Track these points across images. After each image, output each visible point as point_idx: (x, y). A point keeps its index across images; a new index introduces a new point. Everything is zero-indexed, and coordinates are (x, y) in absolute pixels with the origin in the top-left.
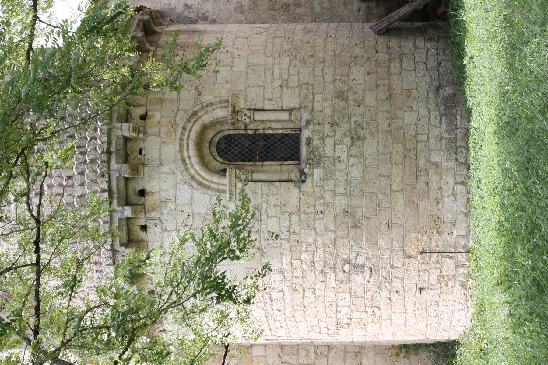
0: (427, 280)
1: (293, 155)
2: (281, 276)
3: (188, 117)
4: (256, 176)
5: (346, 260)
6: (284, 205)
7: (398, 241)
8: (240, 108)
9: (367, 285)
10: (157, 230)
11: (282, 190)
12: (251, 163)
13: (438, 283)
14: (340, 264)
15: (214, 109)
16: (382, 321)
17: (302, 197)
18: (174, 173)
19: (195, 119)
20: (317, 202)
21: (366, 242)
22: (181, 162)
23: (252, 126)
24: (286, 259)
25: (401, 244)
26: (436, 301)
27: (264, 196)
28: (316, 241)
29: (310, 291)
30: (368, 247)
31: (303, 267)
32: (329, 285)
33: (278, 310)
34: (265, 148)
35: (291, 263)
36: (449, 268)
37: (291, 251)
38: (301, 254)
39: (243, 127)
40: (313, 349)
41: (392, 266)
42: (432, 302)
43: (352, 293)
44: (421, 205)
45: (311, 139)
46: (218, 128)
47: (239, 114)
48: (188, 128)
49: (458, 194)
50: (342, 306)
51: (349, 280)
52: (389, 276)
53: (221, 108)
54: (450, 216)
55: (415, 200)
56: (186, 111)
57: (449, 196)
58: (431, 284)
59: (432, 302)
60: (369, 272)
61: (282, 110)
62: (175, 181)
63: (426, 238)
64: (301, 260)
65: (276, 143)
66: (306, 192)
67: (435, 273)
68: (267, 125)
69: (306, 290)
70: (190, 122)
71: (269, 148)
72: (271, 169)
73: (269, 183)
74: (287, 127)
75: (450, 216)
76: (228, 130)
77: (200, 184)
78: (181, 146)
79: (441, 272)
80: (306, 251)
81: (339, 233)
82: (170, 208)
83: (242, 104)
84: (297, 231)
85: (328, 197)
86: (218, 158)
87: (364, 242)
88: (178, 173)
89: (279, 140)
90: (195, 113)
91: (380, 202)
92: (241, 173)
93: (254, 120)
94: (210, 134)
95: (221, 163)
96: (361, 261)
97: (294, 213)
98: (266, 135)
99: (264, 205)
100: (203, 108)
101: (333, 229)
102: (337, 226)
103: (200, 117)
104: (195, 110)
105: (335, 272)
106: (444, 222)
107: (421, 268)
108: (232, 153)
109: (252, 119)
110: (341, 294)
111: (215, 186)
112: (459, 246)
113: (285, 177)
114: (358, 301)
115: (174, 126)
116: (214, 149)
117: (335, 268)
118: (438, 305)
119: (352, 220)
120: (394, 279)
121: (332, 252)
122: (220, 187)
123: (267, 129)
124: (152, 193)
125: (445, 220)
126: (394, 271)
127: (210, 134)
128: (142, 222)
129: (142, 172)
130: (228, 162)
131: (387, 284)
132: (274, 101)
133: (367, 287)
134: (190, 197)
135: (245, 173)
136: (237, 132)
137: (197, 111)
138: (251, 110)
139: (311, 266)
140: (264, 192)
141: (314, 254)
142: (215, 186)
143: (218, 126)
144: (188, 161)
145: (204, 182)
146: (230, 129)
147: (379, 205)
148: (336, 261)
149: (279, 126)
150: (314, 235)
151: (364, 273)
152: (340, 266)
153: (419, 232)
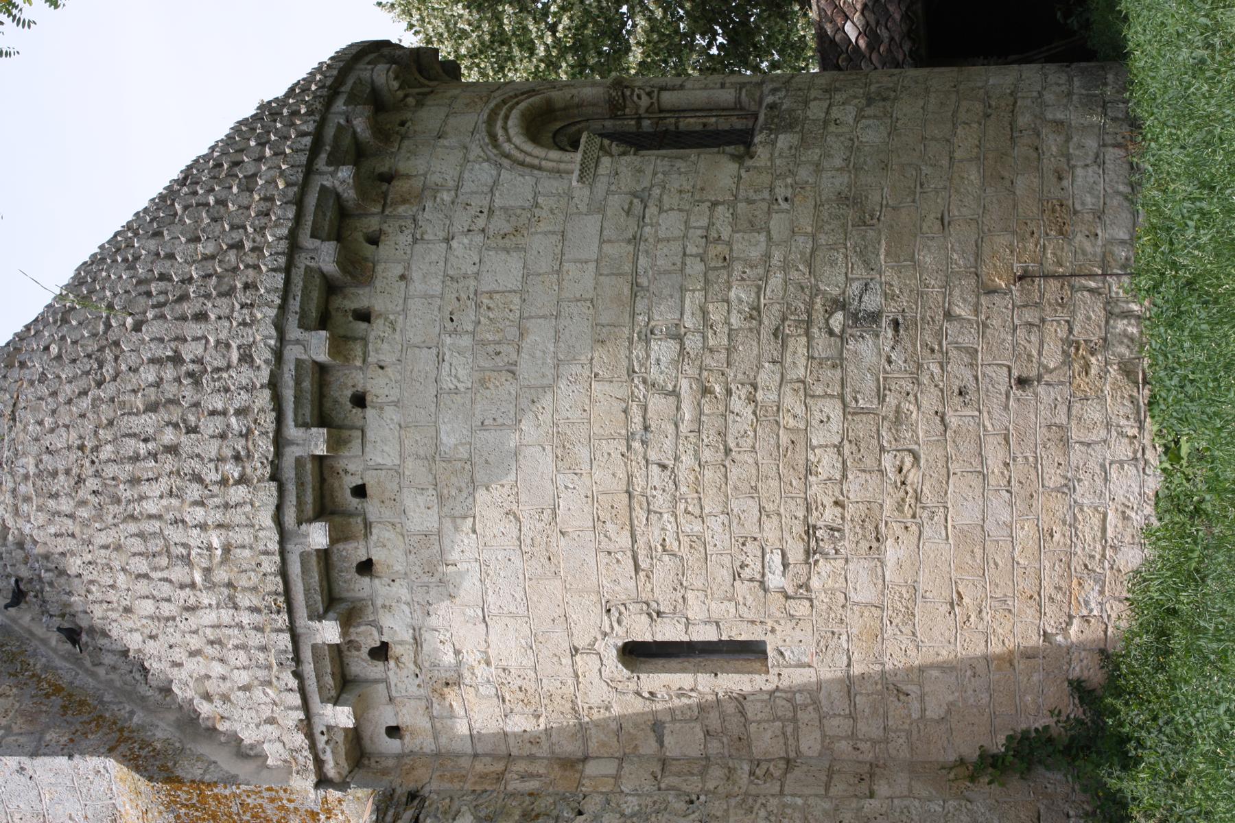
0: (1035, 353)
2: (674, 345)
5: (835, 301)
6: (702, 189)
7: (963, 252)
9: (885, 371)
10: (404, 239)
13: (1064, 363)
14: (821, 310)
16: (925, 515)
17: (743, 174)
20: (778, 183)
21: (886, 255)
24: (692, 301)
25: (972, 259)
26: (1060, 427)
28: (768, 256)
29: (743, 392)
30: (892, 268)
31: (733, 320)
32: (791, 375)
33: (659, 465)
35: (705, 312)
36: (1089, 318)
37: (707, 281)
38: (730, 288)
40: (746, 767)
41: (948, 315)
42: (1049, 427)
43: (848, 399)
44: (1020, 182)
49: (1108, 161)
50: (821, 446)
51: (842, 359)
52: (940, 345)
54: (1089, 200)
55: (1006, 174)
57: (1087, 165)
58: (1046, 367)
59: (1049, 427)
60: (890, 333)
63: (1031, 246)
64: (727, 302)
67: (1055, 332)
69: (734, 389)
75: (1089, 200)
79: (1071, 330)
80: (743, 279)
81: (823, 239)
82: (442, 200)
84: (725, 236)
85: (804, 174)
87: (882, 257)
91: (924, 179)
96: (872, 302)
97: (723, 203)
99: (656, 191)
101: (809, 229)
102: (820, 223)
105: (807, 333)
106: (1076, 212)
107: (1020, 318)
110: (820, 403)
112: (1113, 264)
114: (862, 427)
117: (809, 323)
118: (1065, 442)
119: (856, 211)
120: (953, 353)
121: (804, 281)
124: (408, 176)
125: (1078, 207)
126: (951, 328)
128: (373, 223)
129: (396, 145)
131: (936, 369)
133: (885, 379)
139: (751, 317)
141: (759, 288)
145: (528, 159)
147: (922, 185)
148: (811, 304)
150: (764, 245)
151: (878, 336)
152: (821, 317)
153: (1014, 232)
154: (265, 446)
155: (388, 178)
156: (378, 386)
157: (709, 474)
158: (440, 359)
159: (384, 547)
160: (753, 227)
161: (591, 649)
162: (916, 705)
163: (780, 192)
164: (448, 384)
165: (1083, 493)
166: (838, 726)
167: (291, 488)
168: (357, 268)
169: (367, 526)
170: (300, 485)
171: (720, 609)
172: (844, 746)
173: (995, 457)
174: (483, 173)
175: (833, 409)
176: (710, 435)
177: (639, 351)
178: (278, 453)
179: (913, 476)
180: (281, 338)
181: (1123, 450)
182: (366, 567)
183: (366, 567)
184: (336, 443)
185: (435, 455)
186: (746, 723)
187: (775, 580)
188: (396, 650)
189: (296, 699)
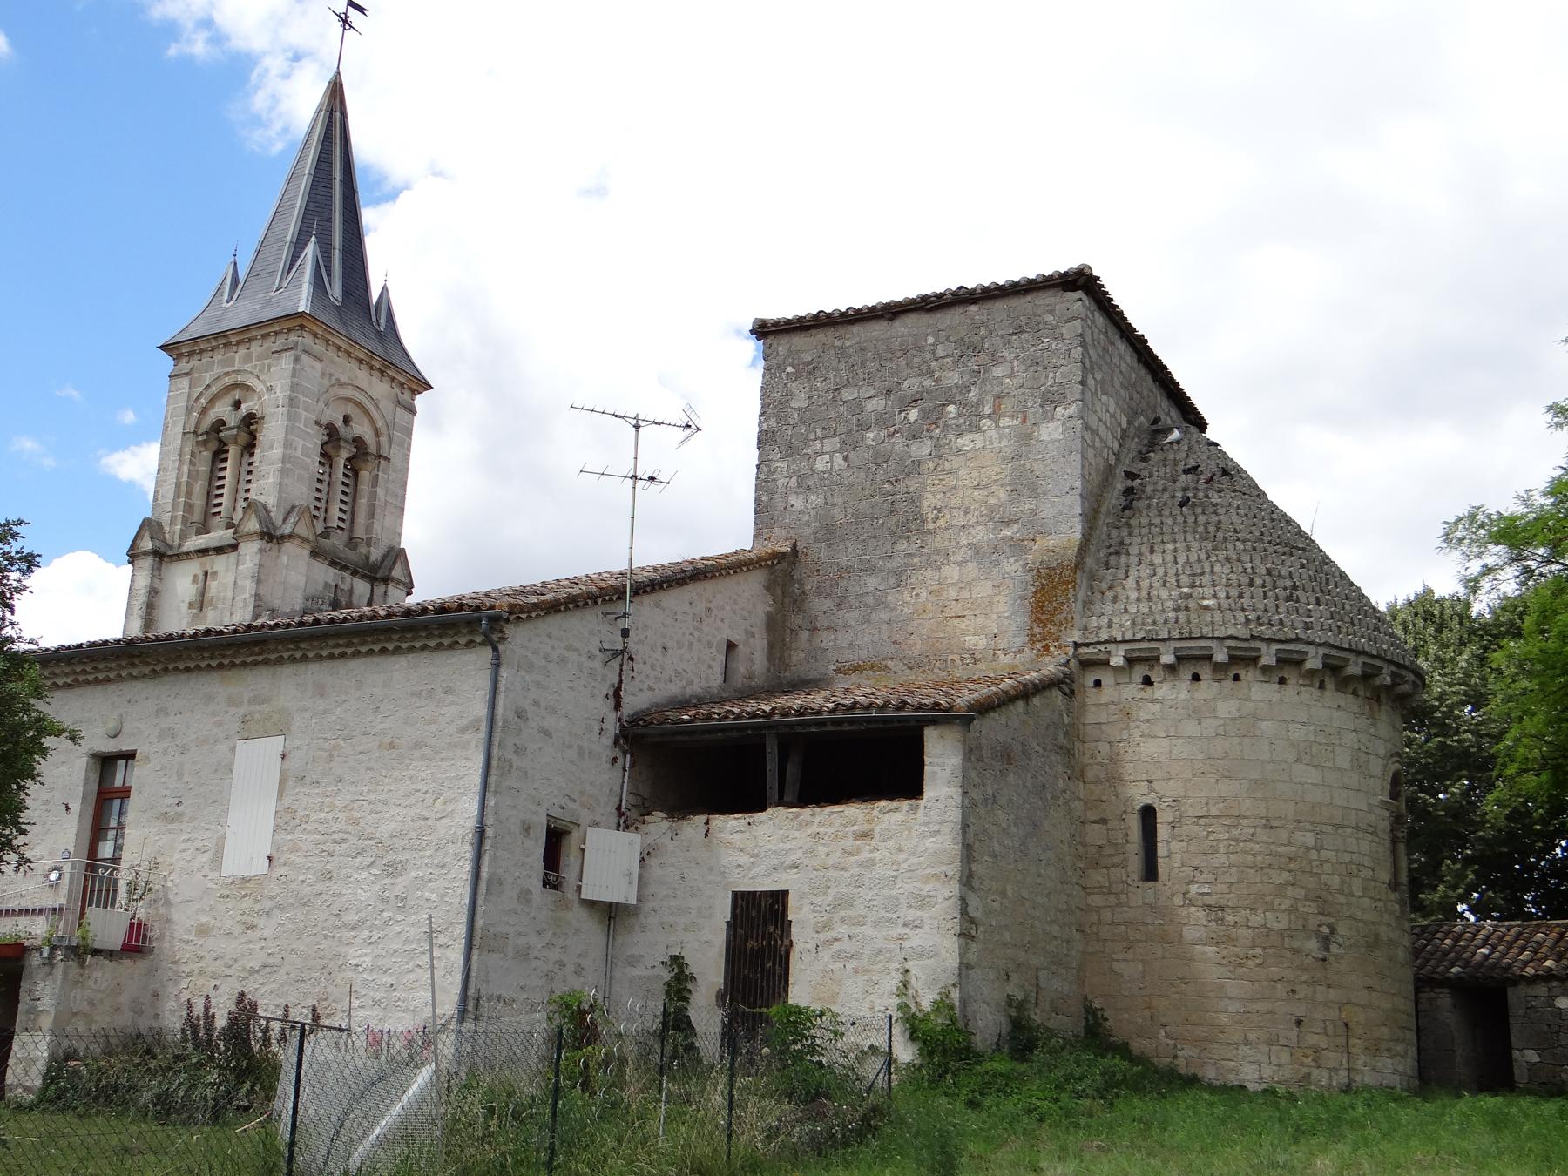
44: (1385, 1030)
96: (1334, 948)
154: (1268, 634)
155: (1378, 701)
156: (1290, 691)
157: (1250, 858)
158: (1303, 724)
159: (1208, 688)
160: (1365, 889)
161: (1152, 790)
162: (1121, 957)
163: (1380, 904)
164: (1292, 727)
165: (1243, 1050)
166: (1107, 915)
167: (1245, 645)
168: (1344, 683)
169: (1219, 680)
170: (1246, 649)
171: (1177, 860)
172: (1095, 918)
173: (1261, 1006)
174: (1382, 752)
175: (1283, 925)
176: (1269, 860)
177: (1308, 826)
178: (1263, 640)
179: (1250, 963)
180: (1319, 645)
181: (1267, 1072)
182: (1196, 678)
183: (1196, 678)
184: (1266, 669)
185: (1257, 718)
186: (1108, 868)
187: (1194, 889)
188: (1149, 689)
189: (1129, 637)
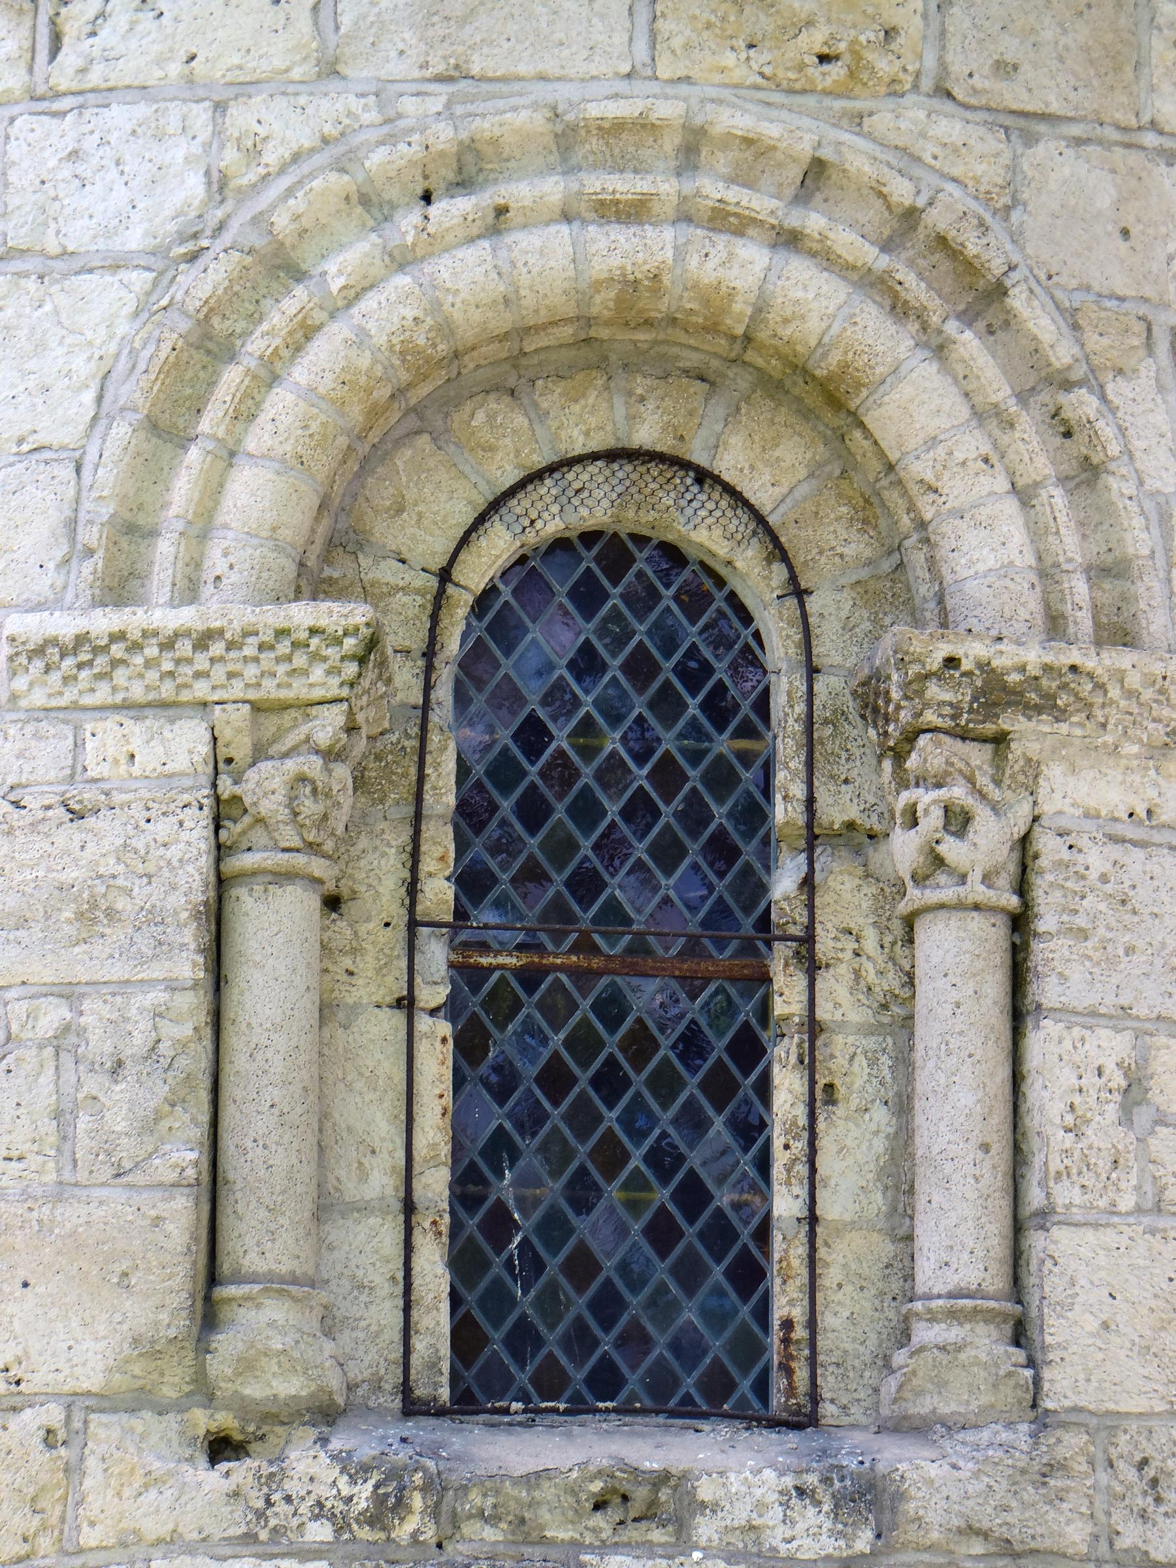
1: (523, 1339)
3: (937, 219)
4: (275, 930)
8: (1033, 768)
11: (107, 1209)
12: (439, 893)
15: (1024, 495)
17: (31, 1420)
18: (330, 69)
19: (915, 288)
22: (444, 135)
23: (846, 898)
27: (53, 1015)
34: (612, 1044)
39: (836, 809)
45: (680, 1525)
46: (834, 547)
47: (978, 756)
48: (813, 222)
53: (1047, 573)
56: (1006, 202)
61: (1018, 1228)
62: (244, 88)
65: (664, 1161)
66: (73, 1471)
68: (851, 1058)
70: (886, 247)
71: (610, 1083)
72: (366, 1102)
73: (198, 1061)
74: (830, 1276)
76: (811, 647)
77: (209, 345)
78: (623, 138)
83: (1079, 784)
86: (497, 548)
88: (331, 108)
89: (693, 1195)
90: (985, 299)
92: (313, 765)
93: (909, 922)
94: (766, 462)
95: (445, 575)
98: (750, 1050)
100: (1045, 382)
103: (940, 350)
104: (1017, 300)
108: (588, 753)
109: (916, 896)
111: (183, 489)
113: (262, 1241)
115: (836, 71)
116: (596, 504)
122: (165, 550)
123: (809, 1063)
127: (766, 462)
130: (452, 645)
132: (1123, 1138)
134: (78, 235)
135: (310, 807)
136: (787, 746)
137: (1008, 321)
138: (1022, 888)
140: (95, 1013)
142: (183, 489)
143: (857, 547)
144: (450, 210)
146: (812, 671)
149: (849, 1187)
